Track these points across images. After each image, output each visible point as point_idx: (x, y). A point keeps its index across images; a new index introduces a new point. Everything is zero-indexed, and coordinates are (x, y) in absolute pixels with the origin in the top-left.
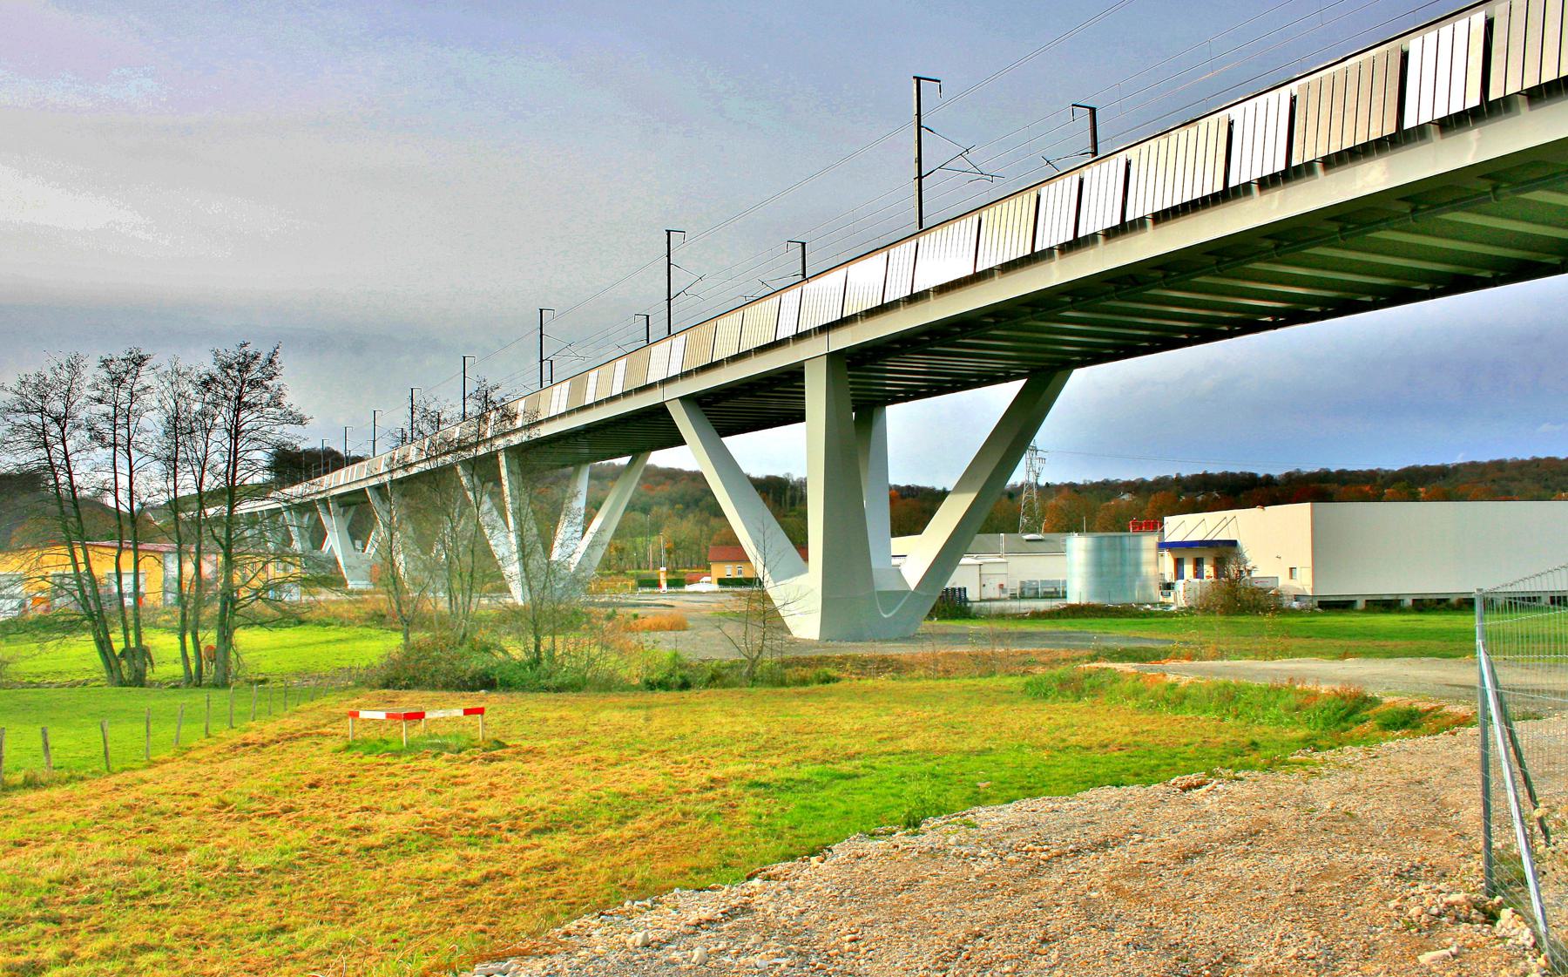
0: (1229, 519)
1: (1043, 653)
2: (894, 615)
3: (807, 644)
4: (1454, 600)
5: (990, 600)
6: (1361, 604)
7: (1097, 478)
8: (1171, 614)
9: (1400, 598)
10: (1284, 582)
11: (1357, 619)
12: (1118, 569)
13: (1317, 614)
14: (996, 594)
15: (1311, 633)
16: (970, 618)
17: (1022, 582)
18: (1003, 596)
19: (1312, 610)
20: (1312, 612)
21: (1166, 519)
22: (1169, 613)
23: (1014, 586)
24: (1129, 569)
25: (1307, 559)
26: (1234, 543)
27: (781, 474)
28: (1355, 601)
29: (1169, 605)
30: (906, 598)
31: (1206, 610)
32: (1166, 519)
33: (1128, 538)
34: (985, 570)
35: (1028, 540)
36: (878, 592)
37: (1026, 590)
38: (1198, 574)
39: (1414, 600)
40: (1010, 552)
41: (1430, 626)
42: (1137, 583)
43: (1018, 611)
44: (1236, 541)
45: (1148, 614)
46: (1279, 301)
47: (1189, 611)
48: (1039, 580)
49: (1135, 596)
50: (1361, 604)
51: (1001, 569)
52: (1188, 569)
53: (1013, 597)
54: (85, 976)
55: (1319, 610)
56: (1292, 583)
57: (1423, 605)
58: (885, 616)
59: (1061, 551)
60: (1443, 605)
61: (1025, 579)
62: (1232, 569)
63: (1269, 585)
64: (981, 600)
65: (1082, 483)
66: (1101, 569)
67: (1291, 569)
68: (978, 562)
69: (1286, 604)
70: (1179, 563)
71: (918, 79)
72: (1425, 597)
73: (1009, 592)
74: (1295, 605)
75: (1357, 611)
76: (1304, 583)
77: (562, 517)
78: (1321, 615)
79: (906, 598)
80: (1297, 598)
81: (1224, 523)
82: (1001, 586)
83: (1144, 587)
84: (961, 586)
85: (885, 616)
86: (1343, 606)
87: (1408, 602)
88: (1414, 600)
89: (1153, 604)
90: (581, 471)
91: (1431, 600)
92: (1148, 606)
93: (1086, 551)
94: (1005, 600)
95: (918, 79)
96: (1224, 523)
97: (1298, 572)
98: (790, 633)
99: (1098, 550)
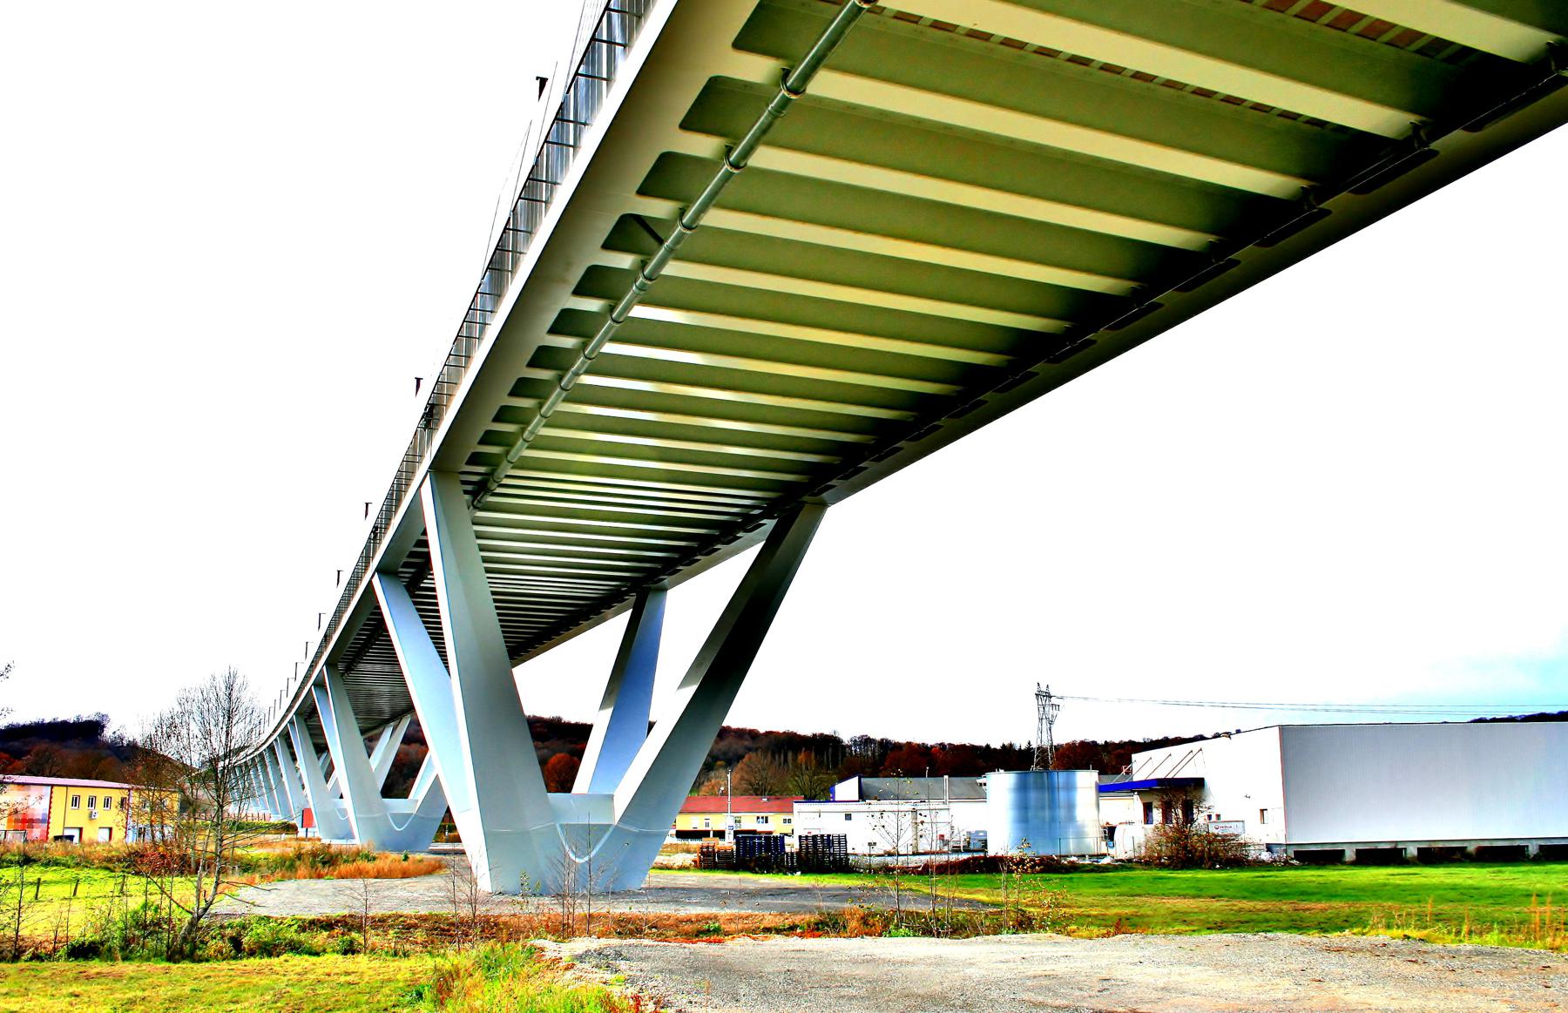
0: (1194, 752)
4: (1471, 848)
6: (1350, 855)
9: (1400, 846)
11: (1332, 873)
12: (1047, 813)
13: (1293, 867)
14: (936, 847)
15: (1246, 894)
17: (969, 833)
18: (946, 849)
19: (1286, 862)
20: (1287, 865)
21: (1133, 755)
22: (1098, 867)
24: (1062, 813)
26: (1199, 783)
27: (827, 732)
28: (1343, 851)
30: (410, 820)
33: (1061, 777)
38: (1166, 818)
41: (1435, 881)
42: (1071, 830)
45: (1073, 868)
46: (419, 558)
49: (1070, 847)
50: (1350, 855)
53: (956, 850)
55: (1294, 862)
57: (1434, 855)
59: (979, 795)
60: (1457, 856)
61: (973, 830)
67: (1262, 811)
69: (1252, 854)
70: (1148, 808)
72: (1433, 845)
74: (1265, 856)
75: (1345, 863)
77: (1195, 811)
79: (410, 820)
80: (1269, 848)
81: (1191, 755)
83: (1080, 835)
86: (1328, 857)
87: (1412, 851)
90: (386, 729)
96: (1191, 755)
99: (1022, 788)
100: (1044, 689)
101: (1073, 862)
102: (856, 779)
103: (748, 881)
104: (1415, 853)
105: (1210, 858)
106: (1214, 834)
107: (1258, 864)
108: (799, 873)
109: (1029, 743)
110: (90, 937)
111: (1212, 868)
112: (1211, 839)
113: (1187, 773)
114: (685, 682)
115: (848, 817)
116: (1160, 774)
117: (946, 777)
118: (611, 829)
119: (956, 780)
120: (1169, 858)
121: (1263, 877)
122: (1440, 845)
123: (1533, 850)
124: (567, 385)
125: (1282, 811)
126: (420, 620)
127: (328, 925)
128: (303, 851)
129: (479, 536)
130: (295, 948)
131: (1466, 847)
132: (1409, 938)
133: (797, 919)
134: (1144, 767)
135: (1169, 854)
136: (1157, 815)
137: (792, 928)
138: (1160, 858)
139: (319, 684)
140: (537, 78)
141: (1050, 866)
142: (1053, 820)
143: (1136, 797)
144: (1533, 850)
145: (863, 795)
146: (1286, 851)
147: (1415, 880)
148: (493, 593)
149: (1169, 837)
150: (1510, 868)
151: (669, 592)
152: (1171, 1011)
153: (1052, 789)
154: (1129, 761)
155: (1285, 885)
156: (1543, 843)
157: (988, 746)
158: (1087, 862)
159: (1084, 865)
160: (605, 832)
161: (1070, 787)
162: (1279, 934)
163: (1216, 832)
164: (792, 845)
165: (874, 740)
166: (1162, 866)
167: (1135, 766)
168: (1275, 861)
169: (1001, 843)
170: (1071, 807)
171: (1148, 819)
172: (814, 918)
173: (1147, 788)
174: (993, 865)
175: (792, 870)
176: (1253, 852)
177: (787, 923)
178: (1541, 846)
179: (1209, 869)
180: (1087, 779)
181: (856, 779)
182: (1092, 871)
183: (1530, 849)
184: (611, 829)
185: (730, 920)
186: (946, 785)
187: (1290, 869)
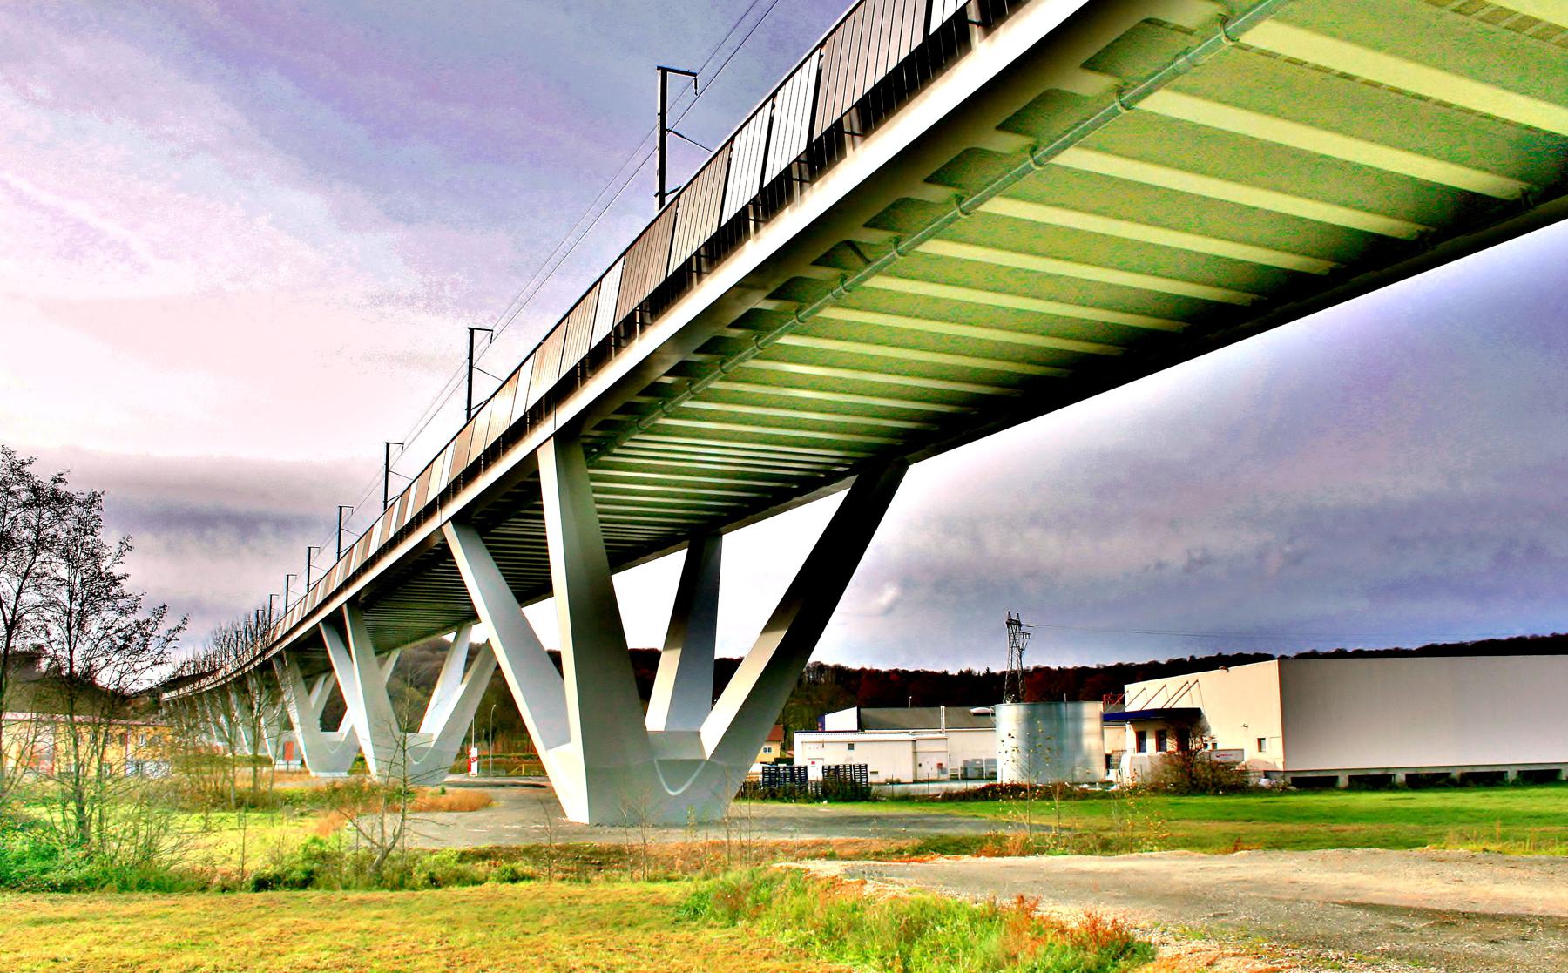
0: (1191, 683)
1: (850, 843)
2: (682, 794)
3: (580, 831)
5: (928, 781)
6: (1343, 781)
7: (1112, 662)
8: (1119, 795)
9: (1390, 773)
10: (1251, 756)
11: (1334, 798)
13: (1289, 793)
16: (868, 800)
17: (965, 762)
18: (943, 777)
19: (1284, 788)
20: (1285, 791)
21: (1127, 687)
23: (957, 766)
25: (1277, 730)
28: (1337, 778)
29: (1110, 783)
31: (1156, 789)
32: (1127, 687)
33: (1068, 708)
34: (921, 747)
35: (976, 714)
36: (660, 762)
37: (969, 770)
38: (1160, 746)
39: (1407, 775)
40: (954, 726)
41: (1425, 804)
43: (926, 793)
44: (1199, 710)
45: (1085, 795)
47: (1134, 791)
48: (984, 758)
50: (1343, 781)
51: (940, 746)
52: (1151, 742)
53: (954, 778)
54: (1046, 972)
55: (1292, 788)
56: (1261, 756)
57: (1420, 781)
58: (672, 793)
60: (1443, 781)
61: (969, 757)
62: (1194, 744)
63: (1232, 759)
64: (915, 782)
65: (1095, 667)
66: (1035, 744)
68: (912, 738)
69: (1253, 781)
70: (1141, 738)
71: (664, 71)
72: (1420, 771)
73: (949, 773)
74: (1264, 782)
75: (1339, 789)
76: (1275, 756)
78: (1295, 794)
80: (1267, 774)
81: (1186, 687)
82: (940, 766)
83: (1086, 763)
84: (862, 763)
85: (672, 793)
86: (1323, 783)
87: (1401, 777)
88: (1407, 775)
89: (1092, 784)
91: (1427, 775)
92: (1086, 786)
93: (1017, 720)
94: (943, 781)
95: (664, 71)
96: (1186, 687)
97: (1266, 744)
98: (564, 815)
99: (1030, 721)
100: (1014, 618)
101: (1085, 789)
102: (855, 710)
103: (806, 810)
104: (1404, 778)
105: (1214, 785)
106: (1216, 762)
107: (1260, 791)
108: (825, 802)
109: (125, 576)
110: (271, 870)
111: (1216, 794)
112: (1214, 767)
113: (1183, 704)
114: (770, 626)
115: (851, 746)
116: (1157, 704)
117: (943, 707)
118: (703, 764)
119: (951, 709)
120: (1175, 785)
121: (1271, 802)
122: (1427, 771)
123: (1512, 775)
124: (727, 368)
125: (1281, 739)
126: (494, 563)
127: (483, 856)
128: (337, 785)
129: (596, 490)
130: (461, 879)
131: (1449, 773)
132: (1487, 851)
133: (903, 844)
134: (1139, 696)
135: (1174, 781)
136: (1151, 742)
137: (900, 852)
138: (1165, 785)
139: (335, 621)
140: (659, 68)
141: (1068, 793)
142: (1061, 749)
143: (1128, 726)
144: (1512, 775)
145: (862, 726)
146: (1283, 777)
147: (1414, 805)
148: (606, 541)
149: (1176, 765)
150: (1499, 793)
151: (724, 537)
152: (746, 970)
153: (1060, 719)
154: (1122, 691)
155: (1307, 809)
156: (1521, 769)
157: (946, 672)
158: (1098, 789)
159: (1096, 793)
160: (697, 767)
161: (1078, 718)
162: (1378, 850)
163: (1218, 760)
164: (815, 774)
165: (827, 666)
166: (1168, 792)
167: (1127, 699)
168: (1273, 787)
169: (1008, 773)
170: (1078, 736)
171: (1141, 747)
172: (918, 842)
173: (1142, 719)
174: (995, 793)
175: (818, 799)
176: (1252, 779)
177: (894, 847)
178: (1519, 772)
179: (1214, 795)
180: (1092, 711)
181: (855, 710)
182: (1103, 797)
183: (1509, 774)
184: (703, 764)
185: (841, 846)
186: (943, 718)
187: (1289, 795)
